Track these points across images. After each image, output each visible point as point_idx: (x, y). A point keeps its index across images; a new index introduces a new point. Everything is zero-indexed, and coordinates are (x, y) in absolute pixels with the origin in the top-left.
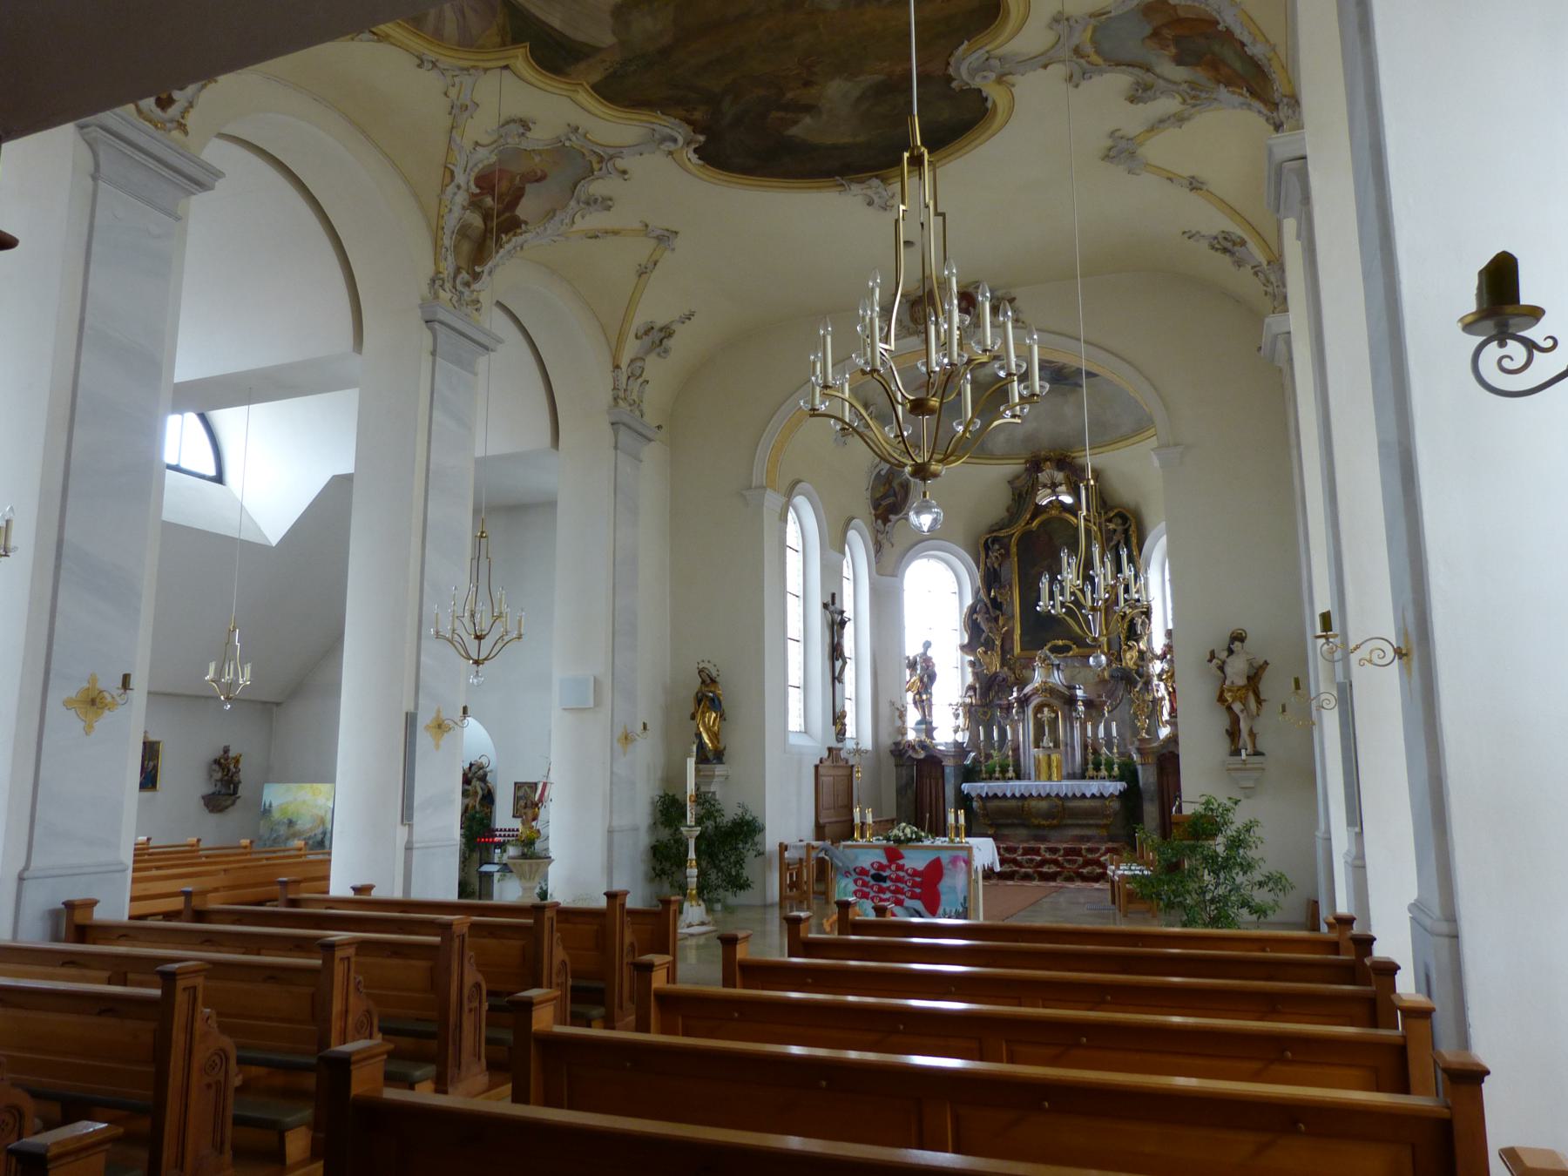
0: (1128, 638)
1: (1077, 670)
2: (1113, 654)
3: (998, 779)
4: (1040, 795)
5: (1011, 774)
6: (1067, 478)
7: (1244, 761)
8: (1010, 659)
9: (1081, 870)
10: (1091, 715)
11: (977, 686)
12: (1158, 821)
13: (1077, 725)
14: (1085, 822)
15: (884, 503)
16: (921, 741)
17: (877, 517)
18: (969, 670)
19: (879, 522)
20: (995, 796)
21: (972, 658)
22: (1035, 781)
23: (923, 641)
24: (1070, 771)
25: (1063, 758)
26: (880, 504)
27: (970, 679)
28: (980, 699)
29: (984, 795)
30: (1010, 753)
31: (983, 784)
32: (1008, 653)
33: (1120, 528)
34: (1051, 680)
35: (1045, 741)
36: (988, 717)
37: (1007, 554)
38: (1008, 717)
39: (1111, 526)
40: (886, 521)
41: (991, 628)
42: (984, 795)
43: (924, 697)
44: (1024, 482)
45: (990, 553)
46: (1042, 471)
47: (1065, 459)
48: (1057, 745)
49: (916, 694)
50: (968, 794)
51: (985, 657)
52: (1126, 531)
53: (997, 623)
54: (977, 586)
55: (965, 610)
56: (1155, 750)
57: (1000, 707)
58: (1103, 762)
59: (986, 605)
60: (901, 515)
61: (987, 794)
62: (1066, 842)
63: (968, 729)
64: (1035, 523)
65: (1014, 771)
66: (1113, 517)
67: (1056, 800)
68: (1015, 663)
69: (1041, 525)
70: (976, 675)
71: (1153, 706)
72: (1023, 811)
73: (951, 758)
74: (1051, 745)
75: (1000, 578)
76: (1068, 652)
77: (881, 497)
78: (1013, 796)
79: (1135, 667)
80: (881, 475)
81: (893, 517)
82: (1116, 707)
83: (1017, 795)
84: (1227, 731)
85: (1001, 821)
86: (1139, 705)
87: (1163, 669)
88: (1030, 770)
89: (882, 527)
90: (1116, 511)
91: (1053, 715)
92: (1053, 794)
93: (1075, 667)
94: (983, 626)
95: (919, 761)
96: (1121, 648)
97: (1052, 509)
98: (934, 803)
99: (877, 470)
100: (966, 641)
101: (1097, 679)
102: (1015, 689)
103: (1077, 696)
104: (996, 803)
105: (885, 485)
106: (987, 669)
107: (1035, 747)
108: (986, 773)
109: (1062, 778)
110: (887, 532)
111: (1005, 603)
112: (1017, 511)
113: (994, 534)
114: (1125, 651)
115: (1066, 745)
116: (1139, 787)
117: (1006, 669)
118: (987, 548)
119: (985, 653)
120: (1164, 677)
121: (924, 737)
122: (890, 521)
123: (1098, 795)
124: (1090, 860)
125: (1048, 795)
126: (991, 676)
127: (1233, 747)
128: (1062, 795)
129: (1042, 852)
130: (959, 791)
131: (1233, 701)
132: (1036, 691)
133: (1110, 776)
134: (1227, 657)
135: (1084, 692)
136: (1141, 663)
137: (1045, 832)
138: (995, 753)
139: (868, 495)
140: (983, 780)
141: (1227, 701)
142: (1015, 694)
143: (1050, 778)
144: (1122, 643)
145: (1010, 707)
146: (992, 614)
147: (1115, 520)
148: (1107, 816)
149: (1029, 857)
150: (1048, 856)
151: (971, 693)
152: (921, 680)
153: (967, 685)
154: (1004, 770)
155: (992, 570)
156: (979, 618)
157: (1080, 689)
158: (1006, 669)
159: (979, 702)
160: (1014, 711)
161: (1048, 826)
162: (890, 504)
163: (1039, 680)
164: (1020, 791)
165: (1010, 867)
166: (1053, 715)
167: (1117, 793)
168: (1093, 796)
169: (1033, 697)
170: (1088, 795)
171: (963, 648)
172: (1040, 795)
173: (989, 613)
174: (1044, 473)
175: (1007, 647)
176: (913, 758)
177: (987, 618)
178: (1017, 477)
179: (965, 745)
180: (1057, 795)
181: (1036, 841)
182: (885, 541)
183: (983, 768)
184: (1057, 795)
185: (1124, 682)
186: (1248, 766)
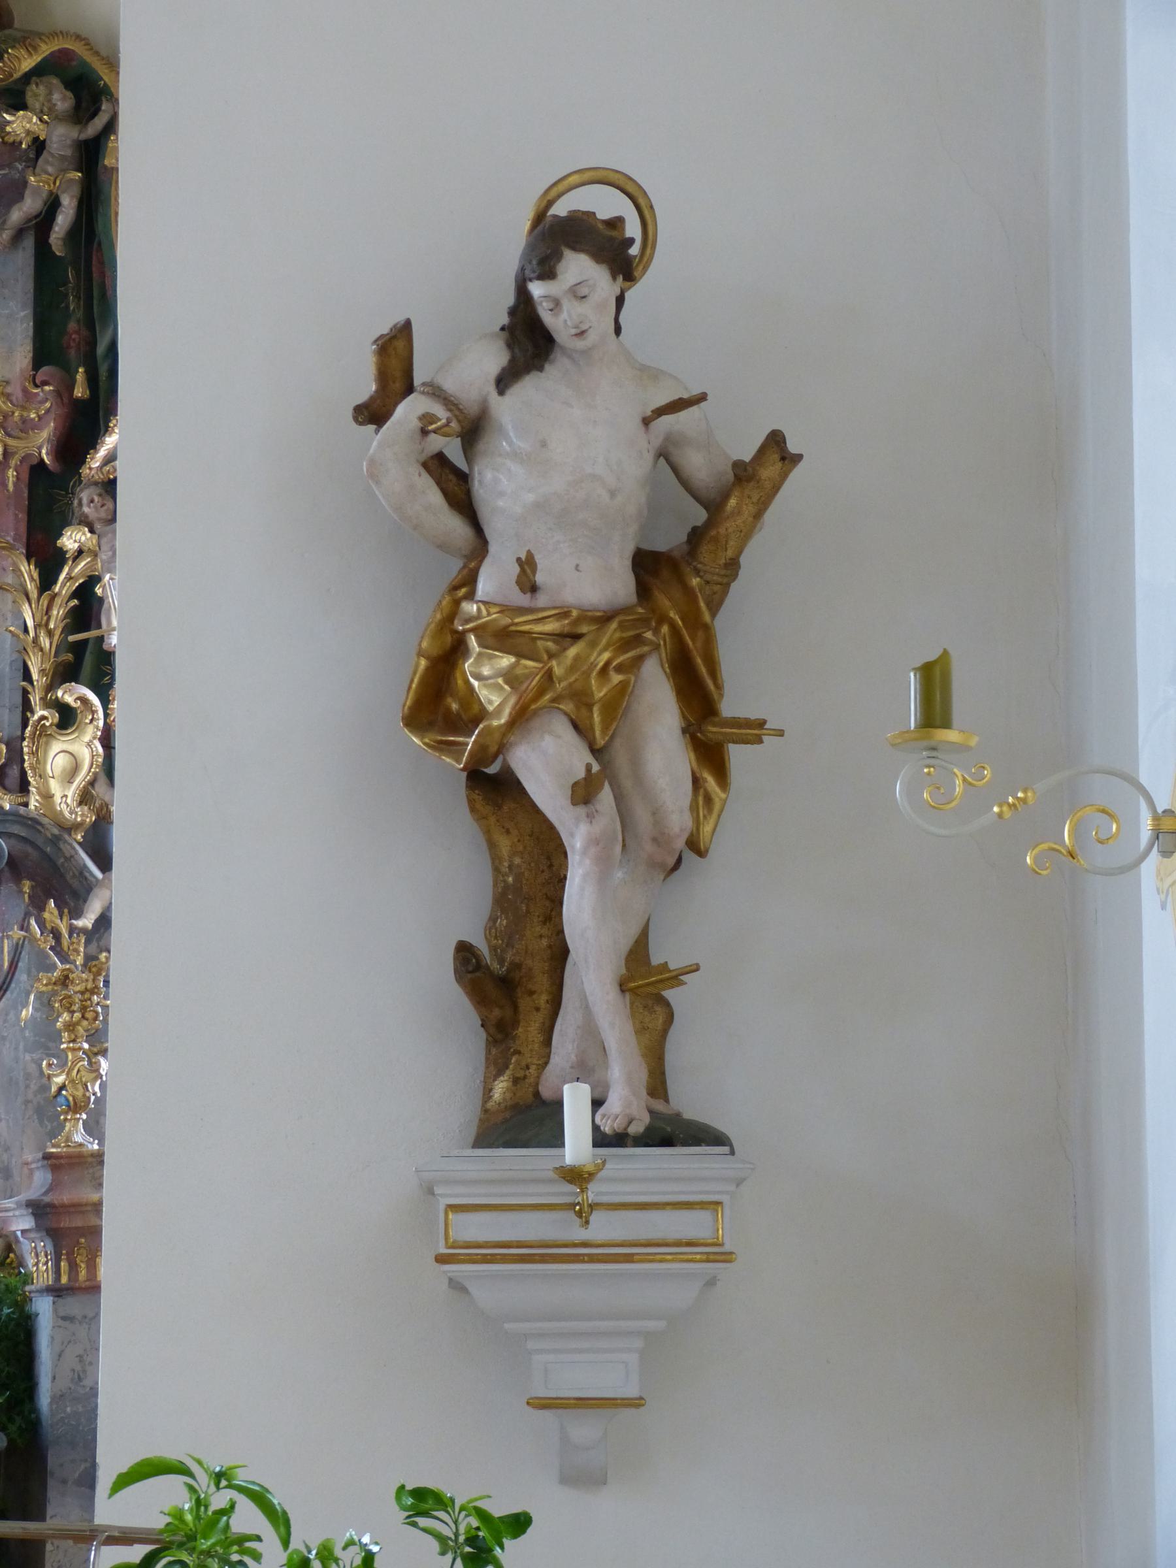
0: (67, 673)
7: (576, 1176)
33: (62, 137)
66: (27, 77)
84: (464, 952)
86: (65, 981)
90: (46, 49)
114: (42, 734)
116: (35, 1410)
127: (500, 1088)
131: (521, 717)
134: (503, 382)
141: (482, 715)
144: (35, 699)
147: (36, 92)
179: (24, 1426)
185: (27, 886)
186: (603, 1227)
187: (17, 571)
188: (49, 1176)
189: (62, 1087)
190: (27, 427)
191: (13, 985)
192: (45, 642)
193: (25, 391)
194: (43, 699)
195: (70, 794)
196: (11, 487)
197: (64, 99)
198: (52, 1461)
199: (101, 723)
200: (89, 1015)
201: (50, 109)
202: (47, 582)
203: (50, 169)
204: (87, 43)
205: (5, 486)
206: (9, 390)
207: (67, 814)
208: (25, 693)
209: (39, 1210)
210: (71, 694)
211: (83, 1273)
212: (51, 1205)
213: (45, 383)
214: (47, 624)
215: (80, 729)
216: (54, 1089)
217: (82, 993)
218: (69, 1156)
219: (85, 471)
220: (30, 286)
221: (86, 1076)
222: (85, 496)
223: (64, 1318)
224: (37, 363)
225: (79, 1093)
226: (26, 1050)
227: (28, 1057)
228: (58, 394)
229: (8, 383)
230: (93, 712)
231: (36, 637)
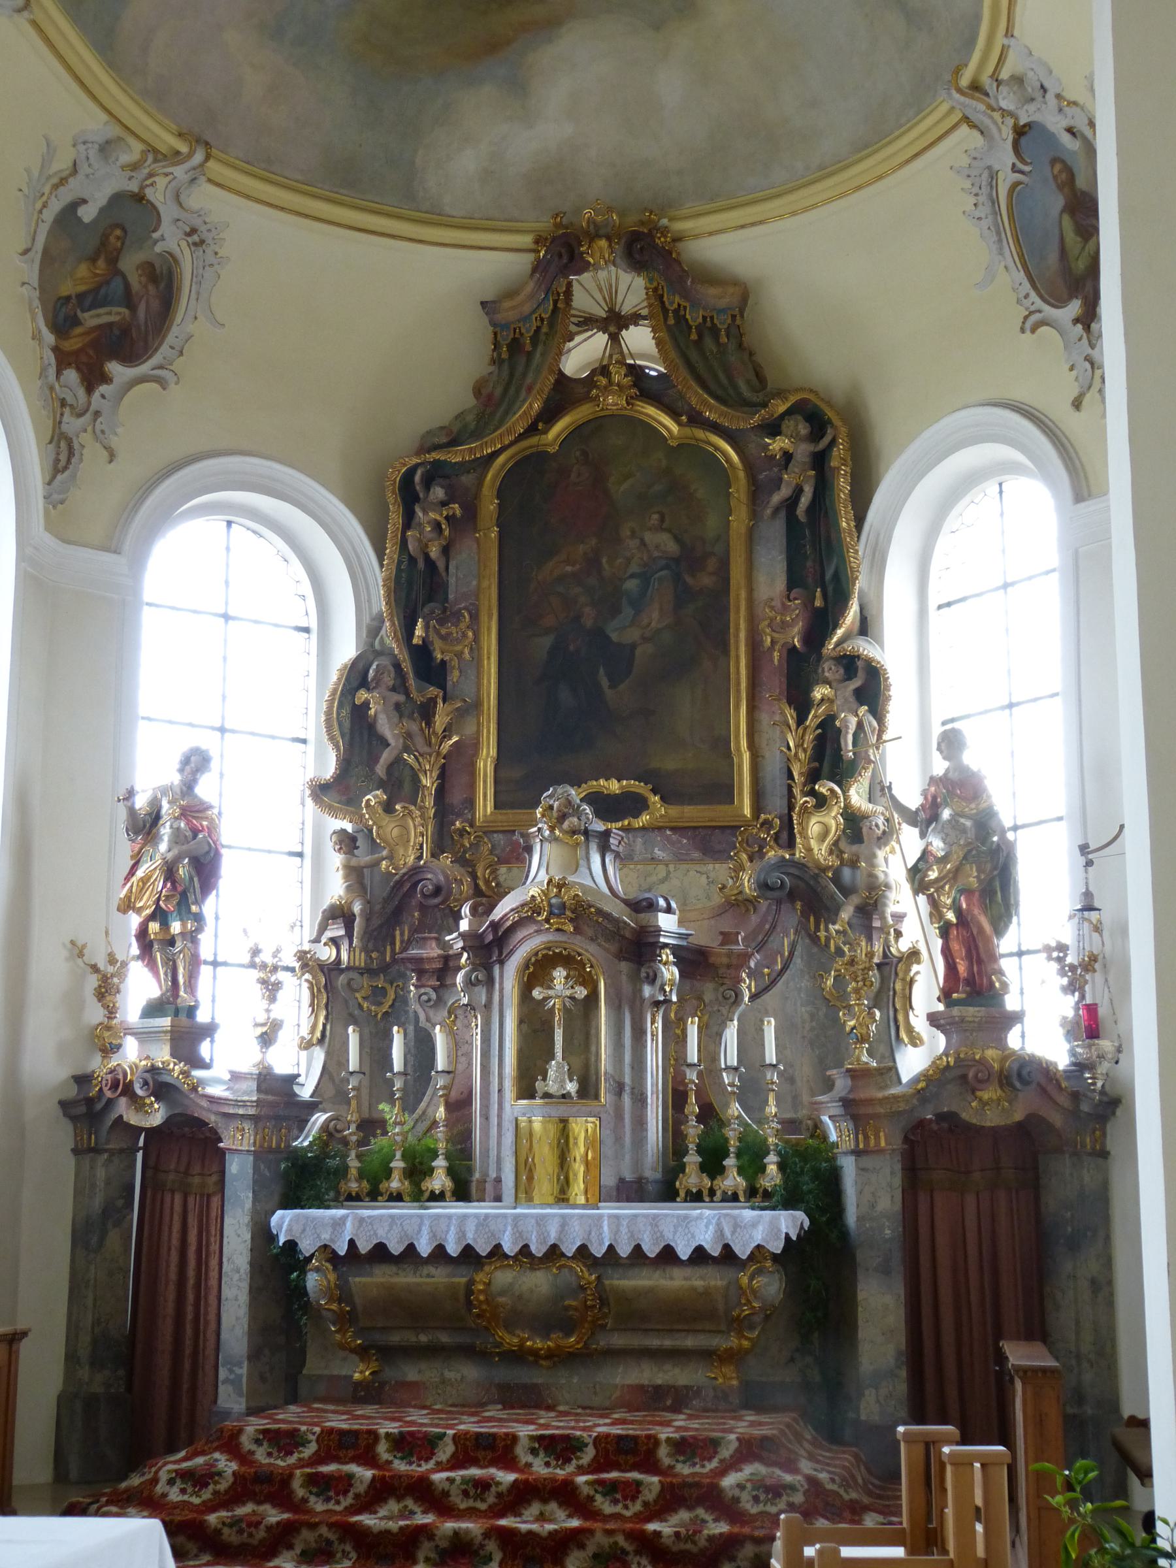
1: (661, 871)
2: (767, 824)
3: (397, 1197)
4: (525, 1250)
5: (439, 1181)
6: (656, 296)
8: (462, 832)
9: (652, 1527)
10: (700, 998)
11: (357, 908)
12: (901, 1339)
13: (655, 1026)
14: (668, 1343)
15: (92, 319)
16: (153, 1070)
17: (63, 359)
18: (335, 860)
19: (72, 376)
20: (380, 1252)
21: (349, 827)
22: (517, 1202)
23: (185, 747)
24: (629, 1176)
25: (607, 1132)
26: (76, 322)
27: (336, 888)
28: (365, 949)
29: (342, 1250)
30: (441, 1113)
31: (339, 1212)
32: (459, 815)
33: (803, 451)
34: (580, 878)
35: (551, 1073)
36: (385, 1008)
37: (469, 519)
38: (440, 1002)
39: (778, 445)
40: (93, 378)
41: (409, 735)
42: (342, 1249)
43: (176, 927)
44: (527, 309)
45: (417, 509)
46: (584, 267)
47: (650, 235)
48: (587, 1090)
49: (152, 917)
50: (291, 1245)
51: (386, 819)
52: (820, 461)
53: (429, 724)
54: (375, 611)
55: (334, 677)
56: (902, 1106)
57: (421, 969)
58: (733, 1144)
59: (397, 666)
60: (144, 368)
61: (352, 1242)
62: (603, 1411)
63: (321, 1041)
64: (560, 427)
65: (450, 1172)
67: (578, 1268)
68: (475, 846)
69: (576, 434)
70: (356, 875)
71: (884, 980)
72: (469, 1303)
73: (247, 1126)
74: (571, 1087)
75: (446, 593)
76: (636, 816)
77: (81, 297)
78: (439, 1252)
79: (833, 861)
80: (79, 220)
81: (114, 368)
82: (773, 982)
83: (453, 1249)
85: (395, 1338)
87: (925, 854)
88: (499, 1169)
89: (81, 392)
90: (793, 399)
91: (581, 992)
92: (570, 1249)
93: (653, 860)
94: (385, 727)
95: (151, 1132)
96: (791, 807)
97: (606, 390)
98: (191, 1273)
99: (66, 195)
100: (329, 770)
101: (718, 899)
102: (466, 910)
103: (658, 931)
104: (381, 1277)
105: (93, 260)
106: (390, 857)
107: (520, 1096)
108: (361, 1175)
109: (600, 1195)
110: (97, 414)
111: (455, 662)
112: (506, 390)
113: (436, 456)
114: (805, 810)
115: (619, 1089)
117: (446, 860)
118: (409, 495)
119: (388, 808)
120: (933, 875)
121: (167, 1057)
122: (106, 379)
123: (715, 1251)
124: (685, 1485)
125: (554, 1252)
126: (399, 884)
128: (598, 1251)
129: (522, 1454)
130: (263, 1235)
132: (530, 912)
133: (752, 1192)
135: (681, 923)
136: (849, 850)
137: (537, 1377)
138: (389, 1112)
139: (31, 271)
140: (353, 1198)
142: (464, 925)
143: (562, 1197)
144: (797, 791)
145: (447, 966)
146: (414, 694)
147: (788, 425)
148: (739, 1325)
149: (475, 1472)
150: (540, 1468)
151: (336, 930)
152: (170, 872)
153: (326, 905)
154: (418, 1170)
155: (421, 565)
156: (375, 702)
157: (669, 910)
158: (446, 860)
159: (360, 960)
160: (459, 978)
161: (550, 1355)
162: (110, 325)
163: (543, 877)
164: (462, 1234)
165: (407, 1514)
166: (581, 992)
167: (777, 1247)
168: (700, 1255)
169: (520, 934)
170: (684, 1253)
171: (321, 791)
172: (525, 1250)
173: (407, 693)
174: (586, 277)
175: (456, 797)
176: (128, 1126)
177: (397, 706)
178: (510, 294)
180: (583, 1251)
181: (507, 1405)
182: (86, 438)
183: (353, 1163)
184: (583, 1251)
185: (799, 905)
187: (783, 713)
188: (849, 1082)
189: (854, 1028)
190: (784, 625)
191: (791, 966)
192: (802, 755)
193: (783, 604)
194: (802, 791)
195: (823, 849)
196: (776, 662)
197: (805, 428)
198: (860, 1256)
199: (842, 805)
200: (867, 983)
201: (797, 435)
202: (801, 720)
203: (796, 470)
204: (816, 393)
205: (772, 661)
206: (773, 604)
207: (822, 861)
208: (790, 788)
209: (848, 1104)
210: (824, 787)
211: (872, 1143)
212: (854, 1100)
213: (796, 599)
214: (802, 745)
215: (830, 809)
216: (848, 1029)
217: (863, 970)
218: (862, 1070)
219: (825, 651)
220: (784, 541)
221: (867, 1020)
222: (826, 666)
223: (863, 1169)
224: (790, 587)
225: (864, 1031)
226: (802, 1005)
227: (803, 1009)
228: (805, 605)
229: (772, 600)
230: (837, 798)
231: (796, 754)
